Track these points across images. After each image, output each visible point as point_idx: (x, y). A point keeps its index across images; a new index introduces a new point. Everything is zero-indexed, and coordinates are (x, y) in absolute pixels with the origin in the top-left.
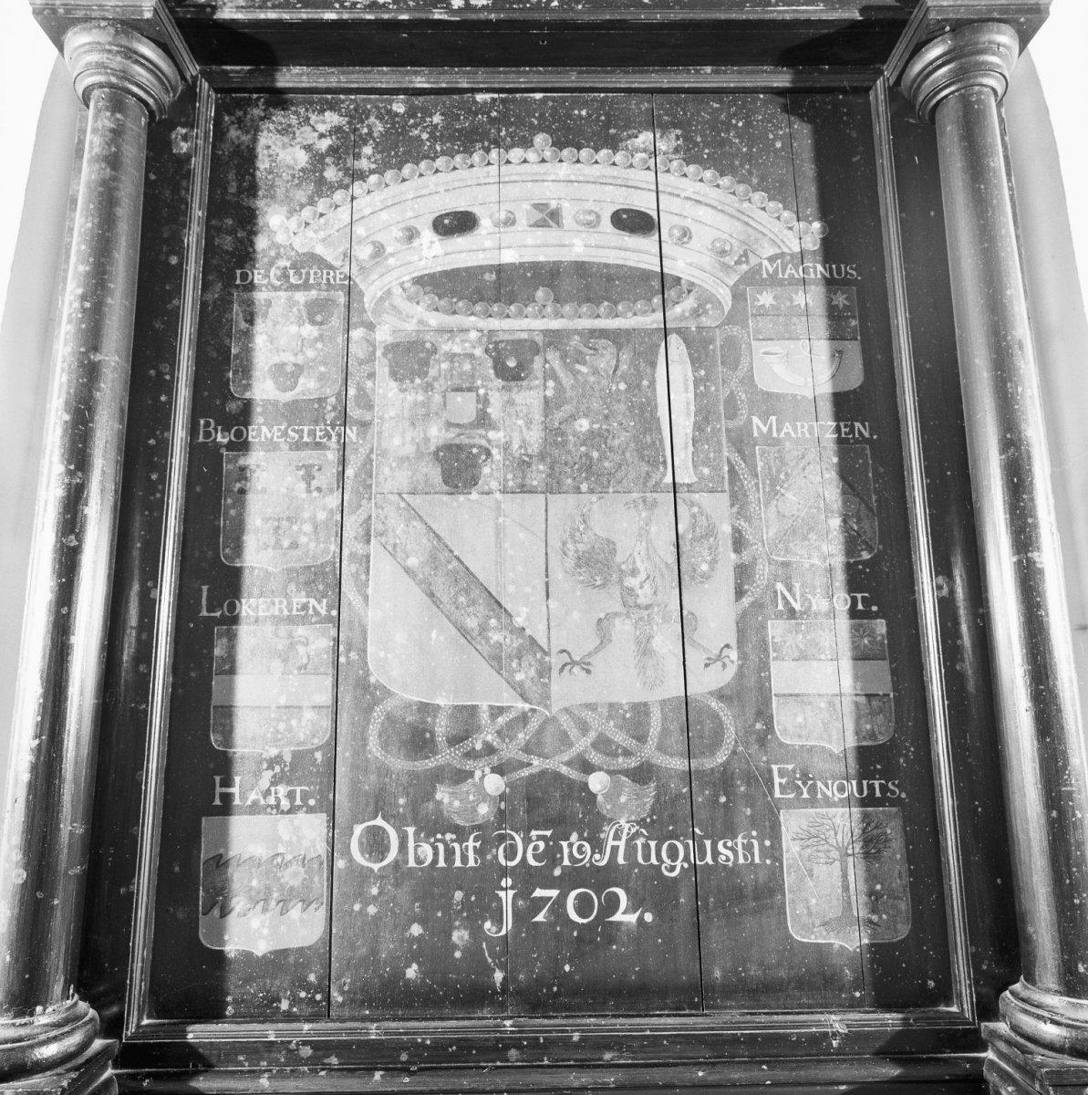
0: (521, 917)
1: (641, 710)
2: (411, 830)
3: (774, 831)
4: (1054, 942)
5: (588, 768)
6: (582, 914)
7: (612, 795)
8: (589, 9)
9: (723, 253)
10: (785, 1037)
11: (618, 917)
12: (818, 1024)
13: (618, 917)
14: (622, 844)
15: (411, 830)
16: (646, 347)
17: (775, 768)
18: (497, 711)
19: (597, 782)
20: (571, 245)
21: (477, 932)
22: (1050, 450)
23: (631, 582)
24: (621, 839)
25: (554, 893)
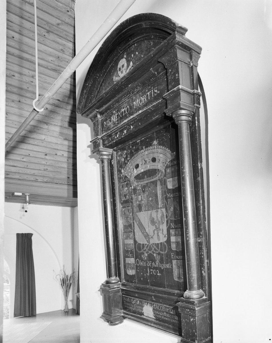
0: (150, 273)
1: (158, 244)
2: (140, 260)
3: (172, 263)
4: (188, 130)
5: (154, 253)
6: (155, 274)
7: (156, 256)
8: (127, 55)
9: (163, 163)
10: (171, 293)
11: (158, 274)
12: (173, 291)
13: (158, 274)
14: (158, 264)
15: (140, 260)
16: (155, 183)
17: (172, 253)
18: (146, 244)
19: (155, 255)
20: (147, 167)
21: (146, 275)
22: (210, 215)
23: (156, 224)
24: (157, 264)
25: (152, 270)
